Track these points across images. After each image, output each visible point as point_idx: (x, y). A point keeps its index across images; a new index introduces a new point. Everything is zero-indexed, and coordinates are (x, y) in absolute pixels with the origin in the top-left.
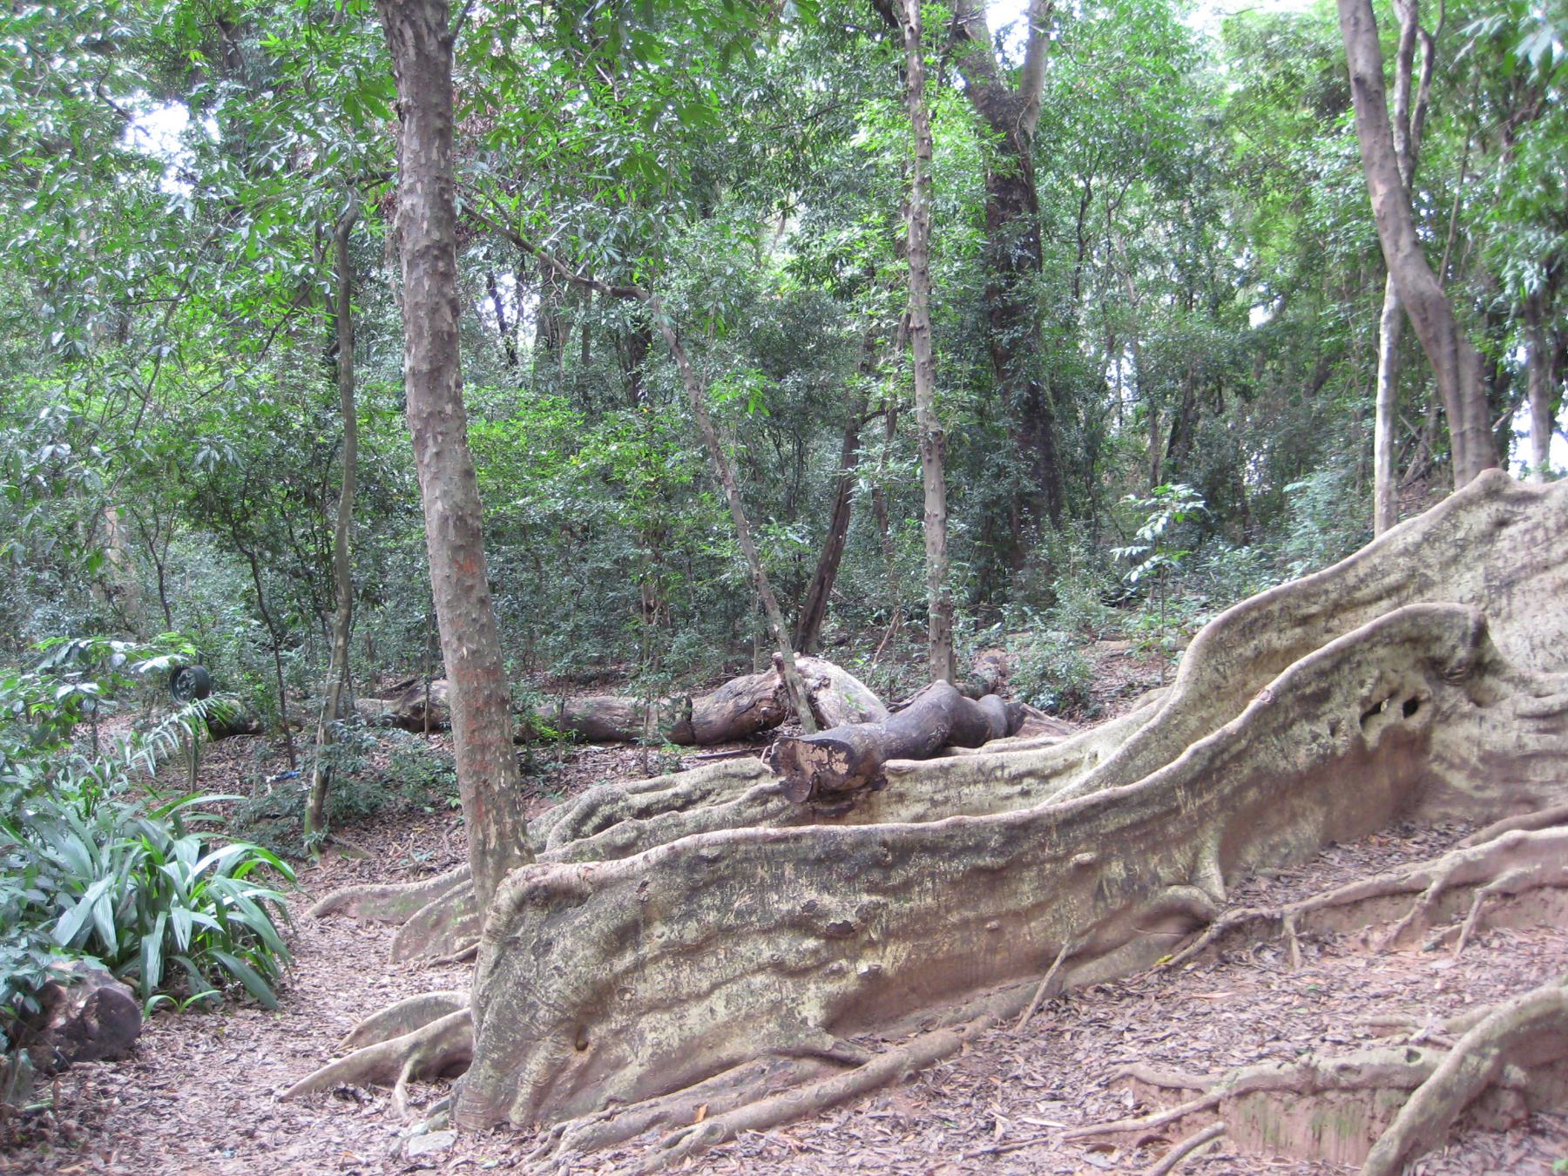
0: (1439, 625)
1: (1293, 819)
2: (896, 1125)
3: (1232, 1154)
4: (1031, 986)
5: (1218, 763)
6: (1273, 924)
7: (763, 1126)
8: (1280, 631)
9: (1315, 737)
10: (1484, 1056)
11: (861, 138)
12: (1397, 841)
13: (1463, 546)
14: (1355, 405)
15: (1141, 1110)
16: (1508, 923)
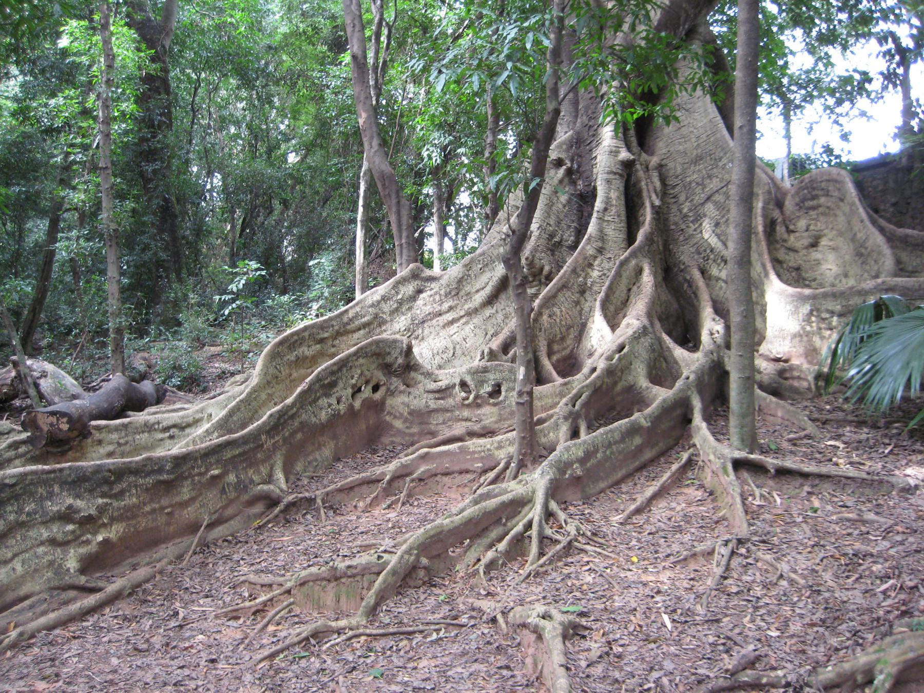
1: (319, 447)
2: (125, 619)
3: (298, 613)
4: (189, 541)
5: (282, 421)
6: (311, 501)
7: (50, 628)
8: (309, 346)
9: (330, 405)
10: (411, 555)
11: (63, 42)
14: (347, 216)
15: (252, 597)
16: (421, 494)
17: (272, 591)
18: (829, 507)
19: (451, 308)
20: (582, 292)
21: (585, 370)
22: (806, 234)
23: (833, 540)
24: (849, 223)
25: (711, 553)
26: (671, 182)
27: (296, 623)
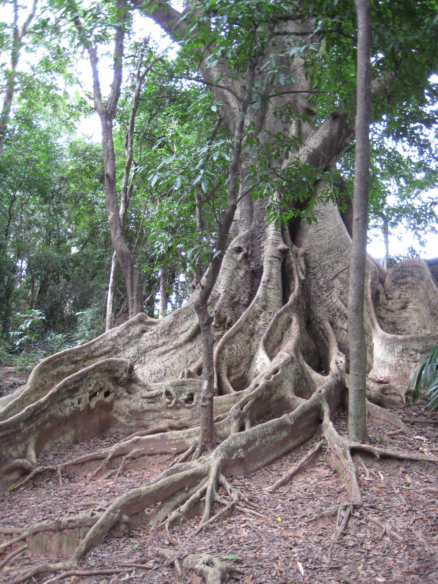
0: (118, 366)
1: (63, 434)
3: (29, 556)
5: (36, 413)
8: (67, 366)
9: (72, 404)
10: (115, 513)
12: (100, 441)
13: (130, 338)
17: (12, 538)
18: (418, 483)
19: (164, 343)
20: (252, 335)
21: (252, 386)
22: (399, 300)
23: (422, 507)
24: (426, 294)
25: (334, 515)
26: (312, 265)
27: (26, 564)
